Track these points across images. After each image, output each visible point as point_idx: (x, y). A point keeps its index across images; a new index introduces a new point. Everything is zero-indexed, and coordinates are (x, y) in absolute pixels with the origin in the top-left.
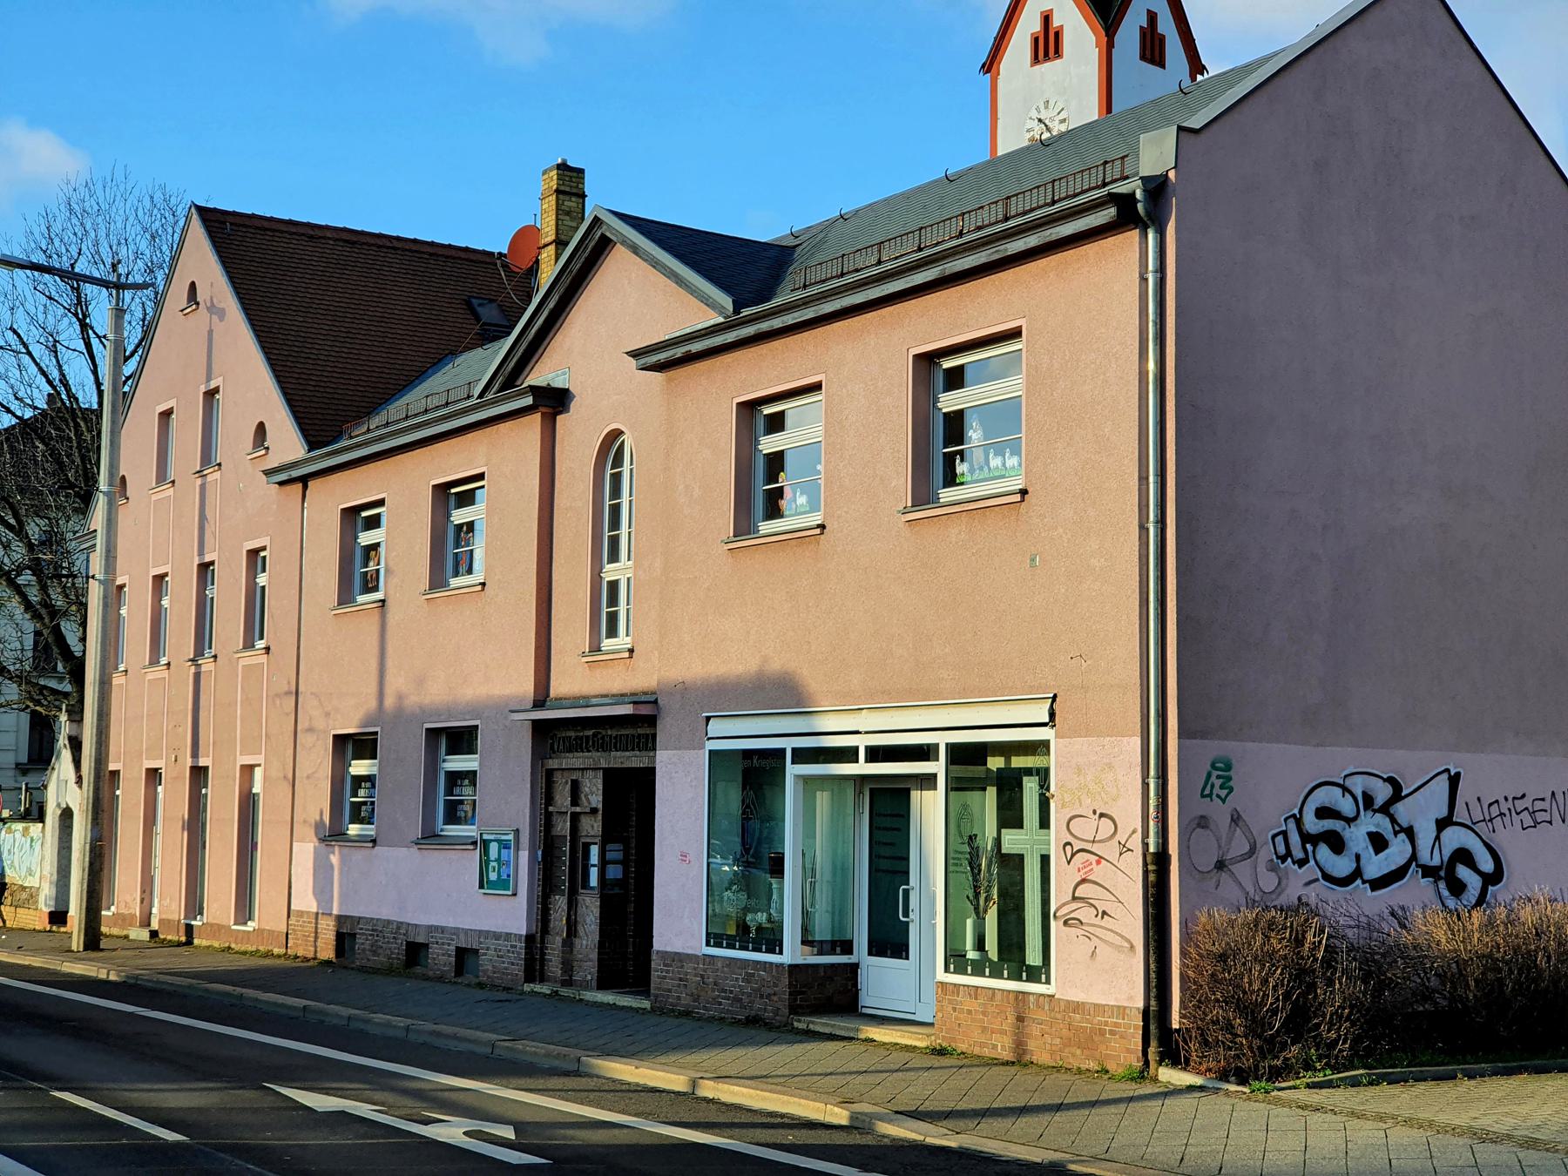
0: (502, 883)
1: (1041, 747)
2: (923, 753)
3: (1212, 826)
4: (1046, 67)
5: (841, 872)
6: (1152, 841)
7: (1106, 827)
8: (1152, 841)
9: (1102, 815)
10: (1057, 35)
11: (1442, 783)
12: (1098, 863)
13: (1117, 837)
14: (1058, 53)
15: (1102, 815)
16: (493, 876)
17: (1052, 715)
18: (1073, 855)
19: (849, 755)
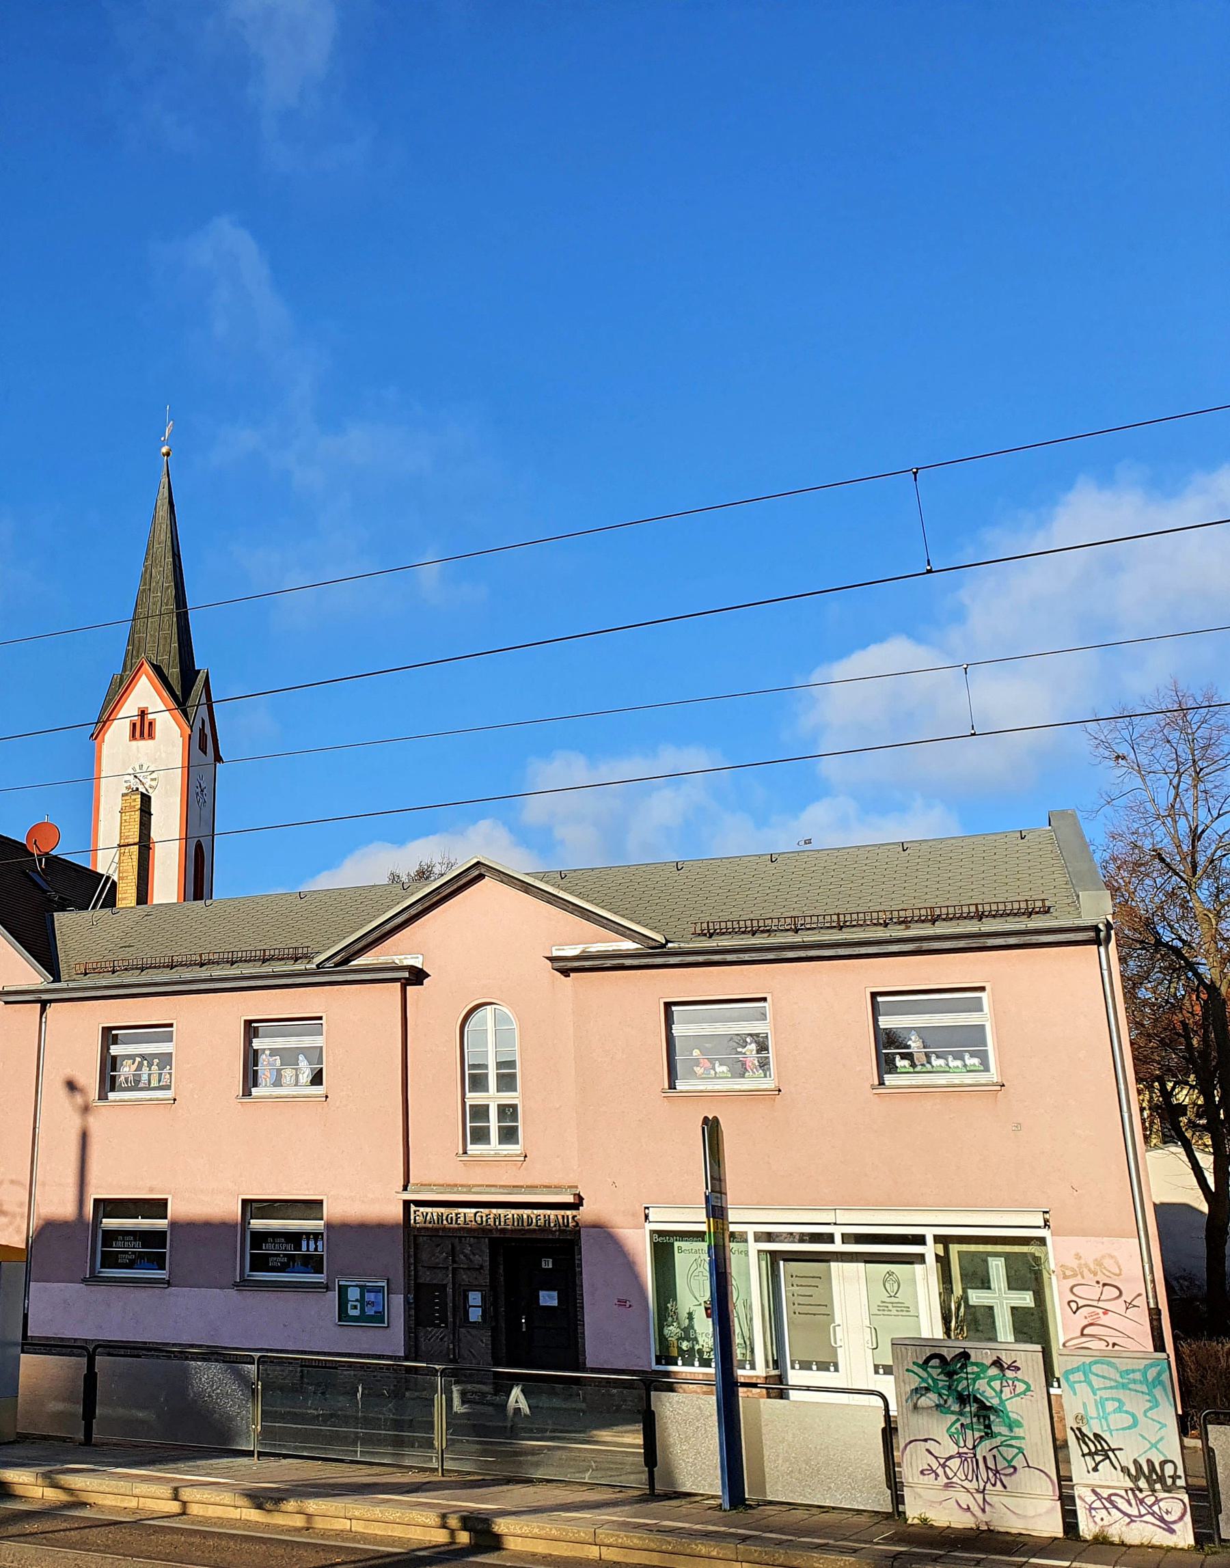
0: (379, 1317)
1: (1042, 1241)
2: (920, 1240)
3: (936, 1413)
4: (142, 744)
5: (101, 1508)
6: (1151, 1301)
7: (1111, 1292)
8: (1151, 1301)
9: (1104, 1285)
10: (150, 724)
11: (1148, 1414)
12: (1105, 1313)
13: (1123, 1298)
14: (151, 736)
15: (1104, 1285)
16: (352, 1312)
17: (1046, 1221)
18: (1078, 1308)
19: (830, 1238)
